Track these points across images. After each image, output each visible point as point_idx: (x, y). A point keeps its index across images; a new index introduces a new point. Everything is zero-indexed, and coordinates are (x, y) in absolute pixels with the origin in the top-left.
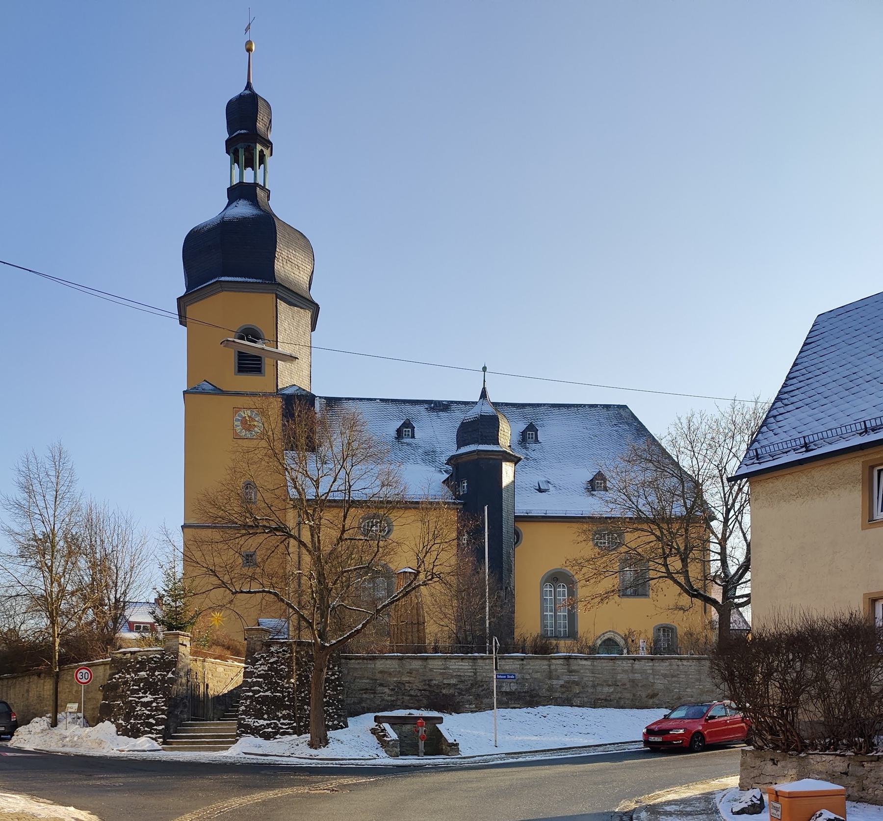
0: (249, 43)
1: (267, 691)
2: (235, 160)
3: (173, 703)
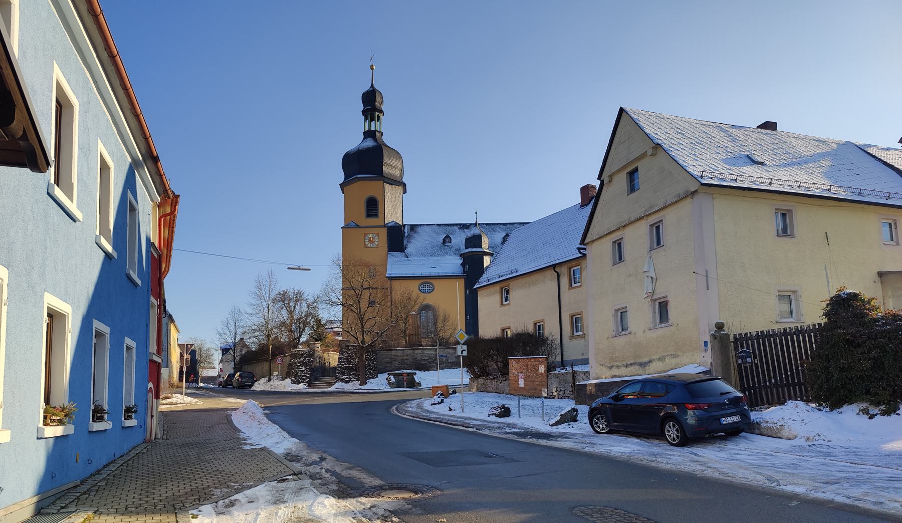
0: (372, 66)
2: (366, 118)
3: (313, 370)
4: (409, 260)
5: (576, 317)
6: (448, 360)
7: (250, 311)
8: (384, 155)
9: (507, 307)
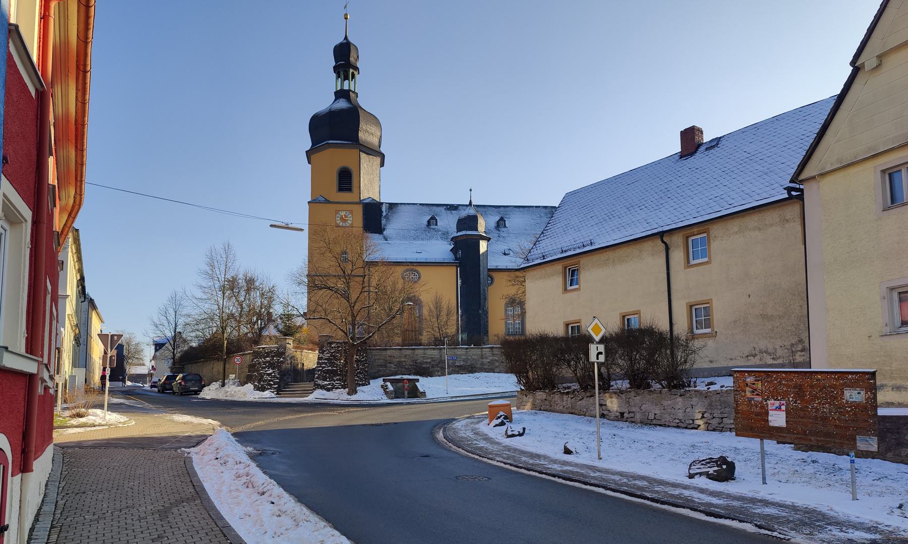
0: (346, 15)
1: (329, 367)
2: (338, 76)
3: (283, 374)
4: (389, 244)
5: (697, 307)
6: (455, 363)
7: (199, 294)
8: (361, 119)
9: (575, 293)
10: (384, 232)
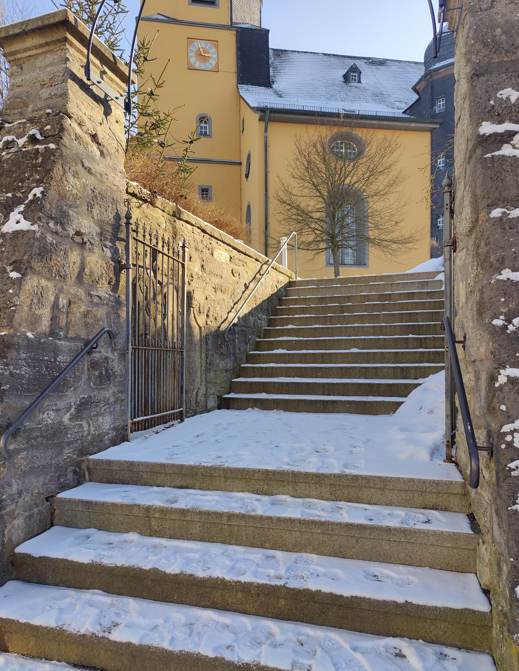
10: (274, 86)
